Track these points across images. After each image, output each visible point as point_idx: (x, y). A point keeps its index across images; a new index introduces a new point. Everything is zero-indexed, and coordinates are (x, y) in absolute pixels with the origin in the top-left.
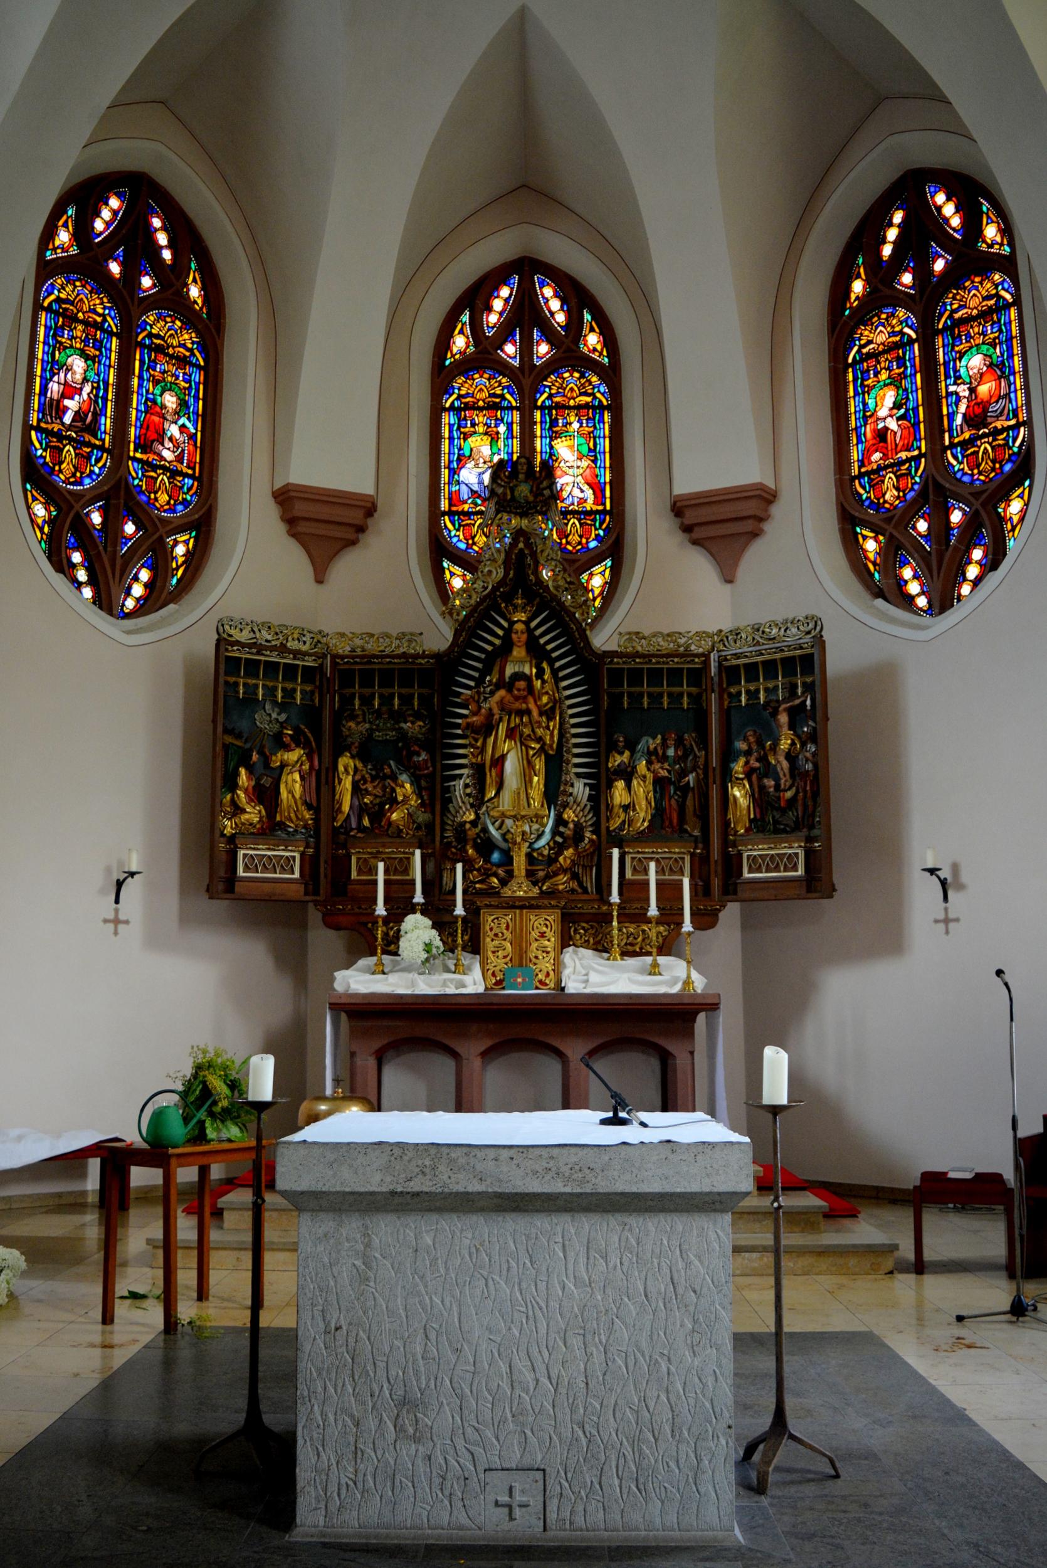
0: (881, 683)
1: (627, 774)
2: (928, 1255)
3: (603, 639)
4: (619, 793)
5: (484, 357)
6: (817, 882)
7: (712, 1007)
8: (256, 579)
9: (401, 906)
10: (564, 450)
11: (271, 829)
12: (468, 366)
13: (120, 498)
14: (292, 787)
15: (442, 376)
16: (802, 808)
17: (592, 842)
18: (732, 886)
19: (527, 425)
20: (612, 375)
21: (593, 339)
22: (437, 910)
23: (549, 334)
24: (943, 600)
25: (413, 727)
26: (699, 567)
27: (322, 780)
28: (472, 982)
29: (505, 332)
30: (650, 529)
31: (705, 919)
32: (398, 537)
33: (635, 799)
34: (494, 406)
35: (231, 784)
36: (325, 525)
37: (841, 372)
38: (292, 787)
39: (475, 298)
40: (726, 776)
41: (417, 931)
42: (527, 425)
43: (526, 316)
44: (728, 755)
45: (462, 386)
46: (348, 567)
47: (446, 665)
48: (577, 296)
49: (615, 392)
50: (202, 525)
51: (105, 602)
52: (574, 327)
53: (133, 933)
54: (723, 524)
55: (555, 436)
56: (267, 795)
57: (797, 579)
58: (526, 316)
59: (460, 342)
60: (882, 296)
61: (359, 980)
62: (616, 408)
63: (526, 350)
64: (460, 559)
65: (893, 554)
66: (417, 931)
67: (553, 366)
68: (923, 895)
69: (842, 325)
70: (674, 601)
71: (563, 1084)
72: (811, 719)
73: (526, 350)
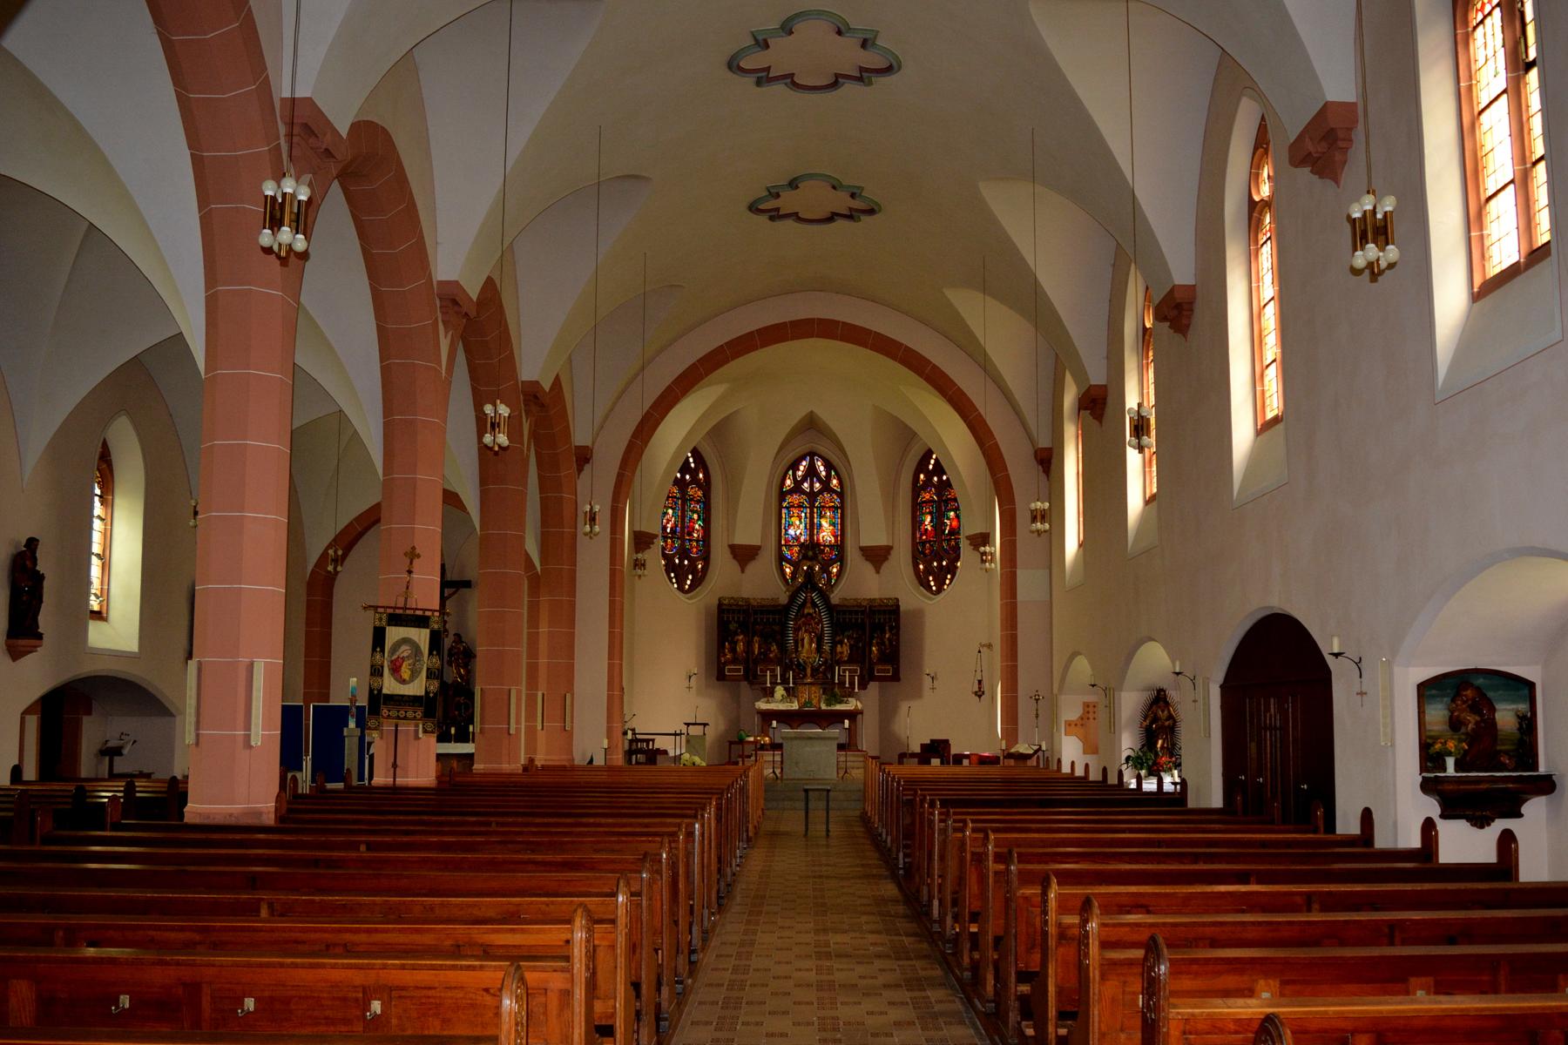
0: (918, 615)
1: (841, 643)
2: (116, 771)
3: (835, 598)
4: (839, 648)
5: (797, 488)
6: (896, 677)
7: (861, 713)
8: (724, 578)
9: (774, 684)
10: (825, 523)
11: (734, 661)
12: (791, 492)
13: (684, 553)
14: (740, 647)
15: (782, 495)
16: (892, 656)
17: (832, 663)
18: (873, 678)
19: (812, 513)
20: (841, 495)
21: (835, 482)
22: (785, 681)
23: (820, 480)
24: (940, 590)
25: (776, 628)
26: (868, 568)
27: (749, 644)
28: (795, 706)
29: (804, 479)
30: (852, 554)
31: (863, 686)
32: (767, 558)
33: (844, 650)
34: (800, 506)
35: (723, 647)
36: (744, 555)
37: (916, 509)
38: (740, 647)
39: (794, 466)
40: (871, 645)
41: (780, 691)
42: (812, 513)
43: (812, 472)
44: (872, 638)
45: (789, 499)
46: (752, 567)
47: (786, 609)
48: (829, 466)
49: (842, 502)
50: (706, 559)
51: (681, 588)
52: (828, 476)
53: (693, 690)
54: (877, 556)
55: (821, 517)
56: (733, 650)
57: (894, 581)
58: (812, 472)
59: (788, 482)
60: (928, 483)
61: (762, 705)
62: (842, 507)
63: (812, 486)
64: (789, 561)
65: (929, 571)
66: (780, 691)
67: (821, 492)
68: (927, 681)
69: (916, 490)
70: (860, 584)
71: (765, 344)
72: (896, 630)
73: (812, 486)
